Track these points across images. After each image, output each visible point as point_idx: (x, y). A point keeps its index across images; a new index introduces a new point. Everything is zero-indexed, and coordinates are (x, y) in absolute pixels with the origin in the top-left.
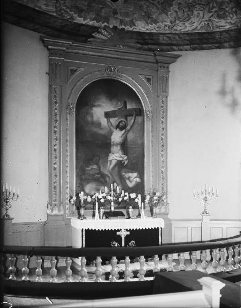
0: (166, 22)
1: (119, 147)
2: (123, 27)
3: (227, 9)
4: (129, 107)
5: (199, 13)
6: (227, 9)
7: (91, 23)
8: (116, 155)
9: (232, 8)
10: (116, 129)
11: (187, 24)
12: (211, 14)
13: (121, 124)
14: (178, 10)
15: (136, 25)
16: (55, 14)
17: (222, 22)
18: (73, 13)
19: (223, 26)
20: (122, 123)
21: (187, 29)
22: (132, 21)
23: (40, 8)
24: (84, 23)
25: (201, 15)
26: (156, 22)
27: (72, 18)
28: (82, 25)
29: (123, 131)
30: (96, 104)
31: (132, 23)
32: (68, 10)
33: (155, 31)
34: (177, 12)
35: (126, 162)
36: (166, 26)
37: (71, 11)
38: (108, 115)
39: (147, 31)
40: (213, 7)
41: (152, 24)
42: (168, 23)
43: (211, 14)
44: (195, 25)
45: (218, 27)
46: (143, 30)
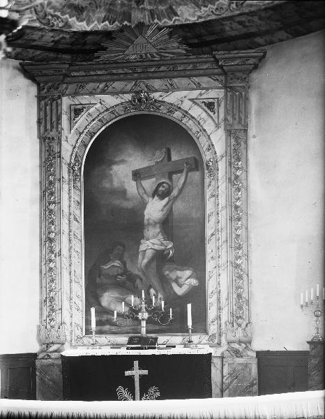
7: (100, 27)
8: (152, 242)
10: (153, 197)
18: (67, 16)
24: (88, 29)
27: (67, 24)
28: (85, 33)
29: (166, 199)
32: (58, 14)
37: (63, 13)
38: (137, 175)
41: (206, 7)
46: (193, 19)
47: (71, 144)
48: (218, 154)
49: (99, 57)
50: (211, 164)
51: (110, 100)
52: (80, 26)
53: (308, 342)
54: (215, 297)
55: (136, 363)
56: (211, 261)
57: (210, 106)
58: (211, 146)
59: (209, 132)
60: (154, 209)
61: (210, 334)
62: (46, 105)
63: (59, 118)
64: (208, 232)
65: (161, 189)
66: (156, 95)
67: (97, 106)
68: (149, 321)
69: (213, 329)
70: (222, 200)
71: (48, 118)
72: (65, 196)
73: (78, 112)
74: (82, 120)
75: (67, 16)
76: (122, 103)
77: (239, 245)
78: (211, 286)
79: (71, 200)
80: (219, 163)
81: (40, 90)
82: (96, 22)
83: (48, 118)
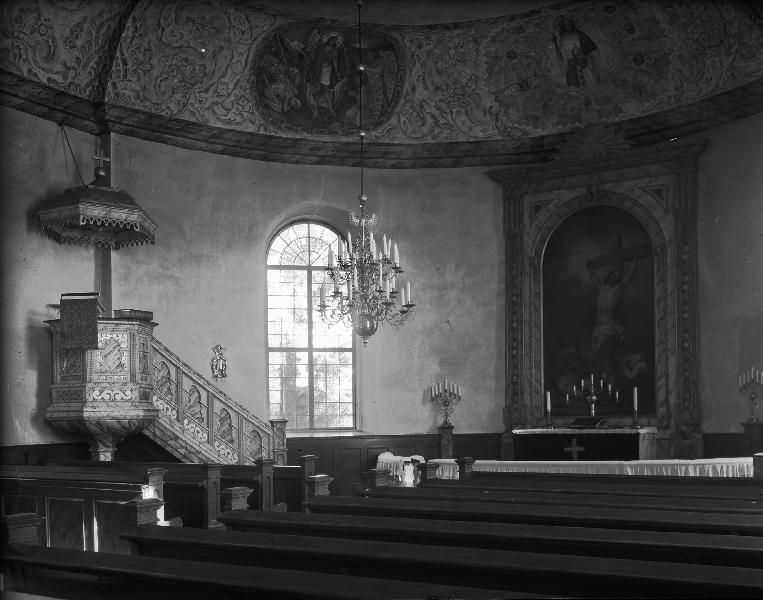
0: (668, 91)
2: (605, 119)
3: (752, 42)
6: (752, 42)
7: (554, 131)
8: (604, 329)
10: (605, 284)
12: (732, 57)
13: (612, 276)
14: (680, 67)
15: (624, 110)
16: (500, 138)
18: (524, 126)
19: (756, 72)
20: (124, 517)
21: (704, 92)
23: (476, 137)
24: (544, 134)
27: (525, 133)
28: (542, 138)
29: (617, 287)
30: (118, 426)
31: (618, 110)
32: (516, 125)
33: (655, 111)
34: (680, 70)
35: (622, 338)
36: (669, 97)
37: (521, 124)
38: (590, 265)
39: (644, 115)
41: (648, 102)
42: (673, 92)
43: (732, 57)
46: (638, 114)
47: (534, 242)
48: (667, 238)
49: (553, 159)
50: (658, 250)
51: (567, 195)
52: (539, 132)
53: (743, 424)
54: (663, 381)
55: (574, 441)
56: (139, 287)
57: (659, 193)
58: (660, 233)
59: (658, 219)
60: (607, 297)
61: (659, 416)
62: (510, 205)
63: (521, 216)
64: (657, 318)
65: (612, 276)
66: (608, 187)
67: (556, 201)
68: (597, 403)
69: (662, 411)
70: (671, 285)
71: (512, 218)
72: (526, 288)
73: (537, 209)
74: (542, 216)
75: (524, 126)
76: (577, 197)
77: (689, 329)
78: (659, 370)
79: (533, 293)
80: (668, 248)
81: (505, 191)
82: (550, 127)
83: (512, 218)
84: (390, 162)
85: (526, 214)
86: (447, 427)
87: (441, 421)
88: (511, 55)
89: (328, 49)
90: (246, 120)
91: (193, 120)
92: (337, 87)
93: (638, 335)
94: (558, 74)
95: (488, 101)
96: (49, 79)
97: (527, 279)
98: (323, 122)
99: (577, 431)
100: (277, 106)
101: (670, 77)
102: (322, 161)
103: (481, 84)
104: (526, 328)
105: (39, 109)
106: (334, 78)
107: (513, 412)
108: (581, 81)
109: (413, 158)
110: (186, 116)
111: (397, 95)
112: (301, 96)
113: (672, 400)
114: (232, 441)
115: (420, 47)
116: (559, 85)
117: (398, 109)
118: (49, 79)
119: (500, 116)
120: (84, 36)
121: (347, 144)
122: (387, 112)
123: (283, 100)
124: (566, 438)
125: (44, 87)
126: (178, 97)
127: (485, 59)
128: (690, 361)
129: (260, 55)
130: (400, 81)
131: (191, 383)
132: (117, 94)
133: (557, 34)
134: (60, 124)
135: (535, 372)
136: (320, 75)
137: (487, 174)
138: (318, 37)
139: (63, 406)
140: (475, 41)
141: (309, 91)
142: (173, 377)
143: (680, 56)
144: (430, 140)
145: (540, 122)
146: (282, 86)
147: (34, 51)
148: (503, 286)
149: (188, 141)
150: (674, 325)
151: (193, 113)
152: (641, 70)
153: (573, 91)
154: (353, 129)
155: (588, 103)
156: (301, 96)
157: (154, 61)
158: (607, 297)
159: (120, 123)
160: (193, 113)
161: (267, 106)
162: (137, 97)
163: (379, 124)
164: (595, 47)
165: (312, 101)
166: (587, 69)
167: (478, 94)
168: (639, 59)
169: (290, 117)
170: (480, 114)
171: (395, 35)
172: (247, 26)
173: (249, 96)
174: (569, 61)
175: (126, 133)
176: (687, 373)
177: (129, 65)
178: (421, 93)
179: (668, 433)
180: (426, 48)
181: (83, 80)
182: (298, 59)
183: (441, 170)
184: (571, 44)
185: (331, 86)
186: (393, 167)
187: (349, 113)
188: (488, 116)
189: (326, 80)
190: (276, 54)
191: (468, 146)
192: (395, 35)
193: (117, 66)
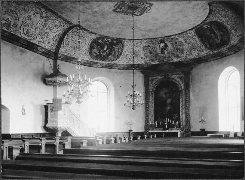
1: (170, 105)
4: (173, 90)
5: (194, 52)
9: (204, 48)
11: (191, 56)
16: (144, 64)
17: (203, 53)
21: (192, 58)
22: (172, 59)
24: (155, 64)
25: (195, 52)
26: (180, 57)
27: (150, 63)
34: (187, 53)
36: (184, 58)
38: (165, 94)
40: (198, 49)
42: (185, 57)
44: (194, 56)
45: (202, 55)
46: (177, 61)
51: (160, 78)
52: (153, 63)
54: (182, 120)
55: (163, 134)
58: (181, 87)
60: (169, 101)
63: (149, 82)
64: (181, 106)
66: (169, 76)
69: (182, 127)
70: (184, 99)
74: (154, 82)
77: (188, 109)
79: (151, 99)
84: (118, 68)
85: (150, 81)
86: (130, 131)
87: (129, 129)
88: (149, 46)
89: (107, 42)
90: (88, 58)
91: (76, 57)
92: (108, 51)
93: (176, 110)
94: (159, 51)
95: (142, 56)
96: (48, 48)
97: (150, 96)
98: (104, 59)
99: (164, 131)
100: (94, 54)
101: (184, 54)
102: (102, 67)
103: (141, 52)
104: (150, 108)
105: (109, 67)
106: (107, 49)
107: (147, 127)
108: (164, 53)
109: (124, 67)
110: (74, 56)
111: (121, 54)
112: (99, 52)
113: (184, 124)
114: (85, 133)
115: (128, 43)
116: (159, 53)
117: (121, 56)
118: (48, 48)
119: (145, 59)
120: (56, 38)
121: (109, 63)
122: (119, 56)
123: (95, 53)
124: (162, 133)
125: (47, 49)
126: (73, 52)
127: (143, 47)
128: (188, 116)
129: (92, 43)
130: (122, 50)
131: (76, 119)
132: (61, 51)
133: (160, 42)
134: (47, 58)
135: (152, 118)
136: (104, 48)
137: (141, 72)
138: (105, 40)
139: (51, 124)
140: (141, 43)
141: (101, 51)
142: (73, 117)
143: (187, 50)
144: (128, 64)
145: (154, 61)
146: (95, 50)
147: (46, 42)
148: (144, 98)
149: (74, 62)
150: (184, 108)
151: (76, 56)
152: (178, 52)
153: (162, 55)
154: (110, 60)
155: (165, 57)
156: (99, 52)
157: (69, 44)
158: (169, 101)
159: (60, 58)
160: (76, 56)
161: (92, 54)
162: (65, 52)
163: (116, 59)
164: (168, 46)
165: (102, 54)
166: (166, 50)
167: (140, 54)
168: (177, 49)
169: (97, 57)
170: (140, 58)
171: (123, 40)
172: (91, 37)
173: (88, 52)
174: (162, 48)
175: (61, 60)
176: (187, 118)
177: (65, 44)
178: (127, 53)
179: (183, 131)
180: (129, 43)
181: (54, 48)
182: (99, 44)
183: (129, 70)
184: (162, 45)
185: (107, 50)
186: (118, 69)
187: (110, 57)
188: (142, 59)
189: (105, 49)
190: (95, 43)
191: (136, 65)
192: (123, 40)
193: (62, 45)
